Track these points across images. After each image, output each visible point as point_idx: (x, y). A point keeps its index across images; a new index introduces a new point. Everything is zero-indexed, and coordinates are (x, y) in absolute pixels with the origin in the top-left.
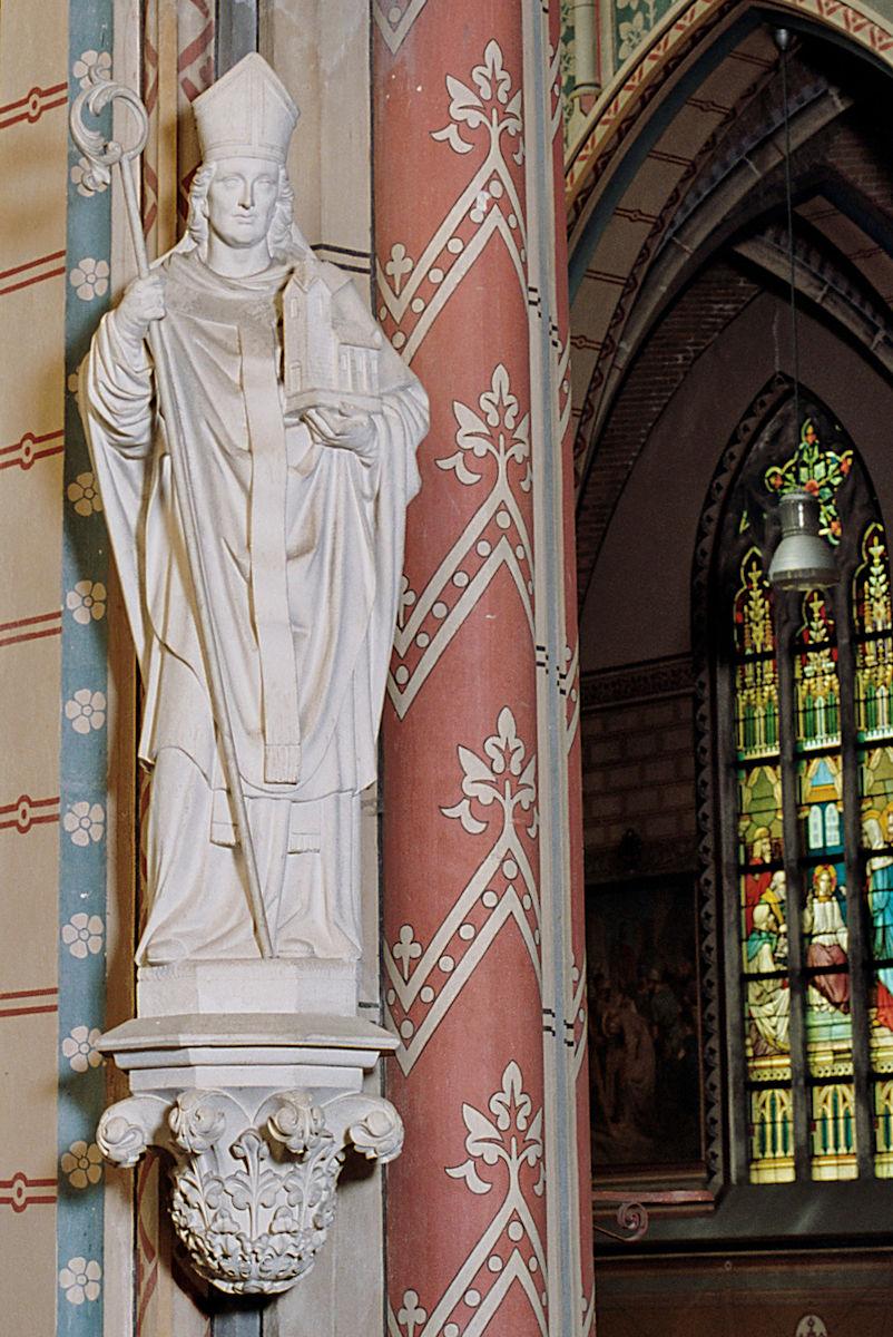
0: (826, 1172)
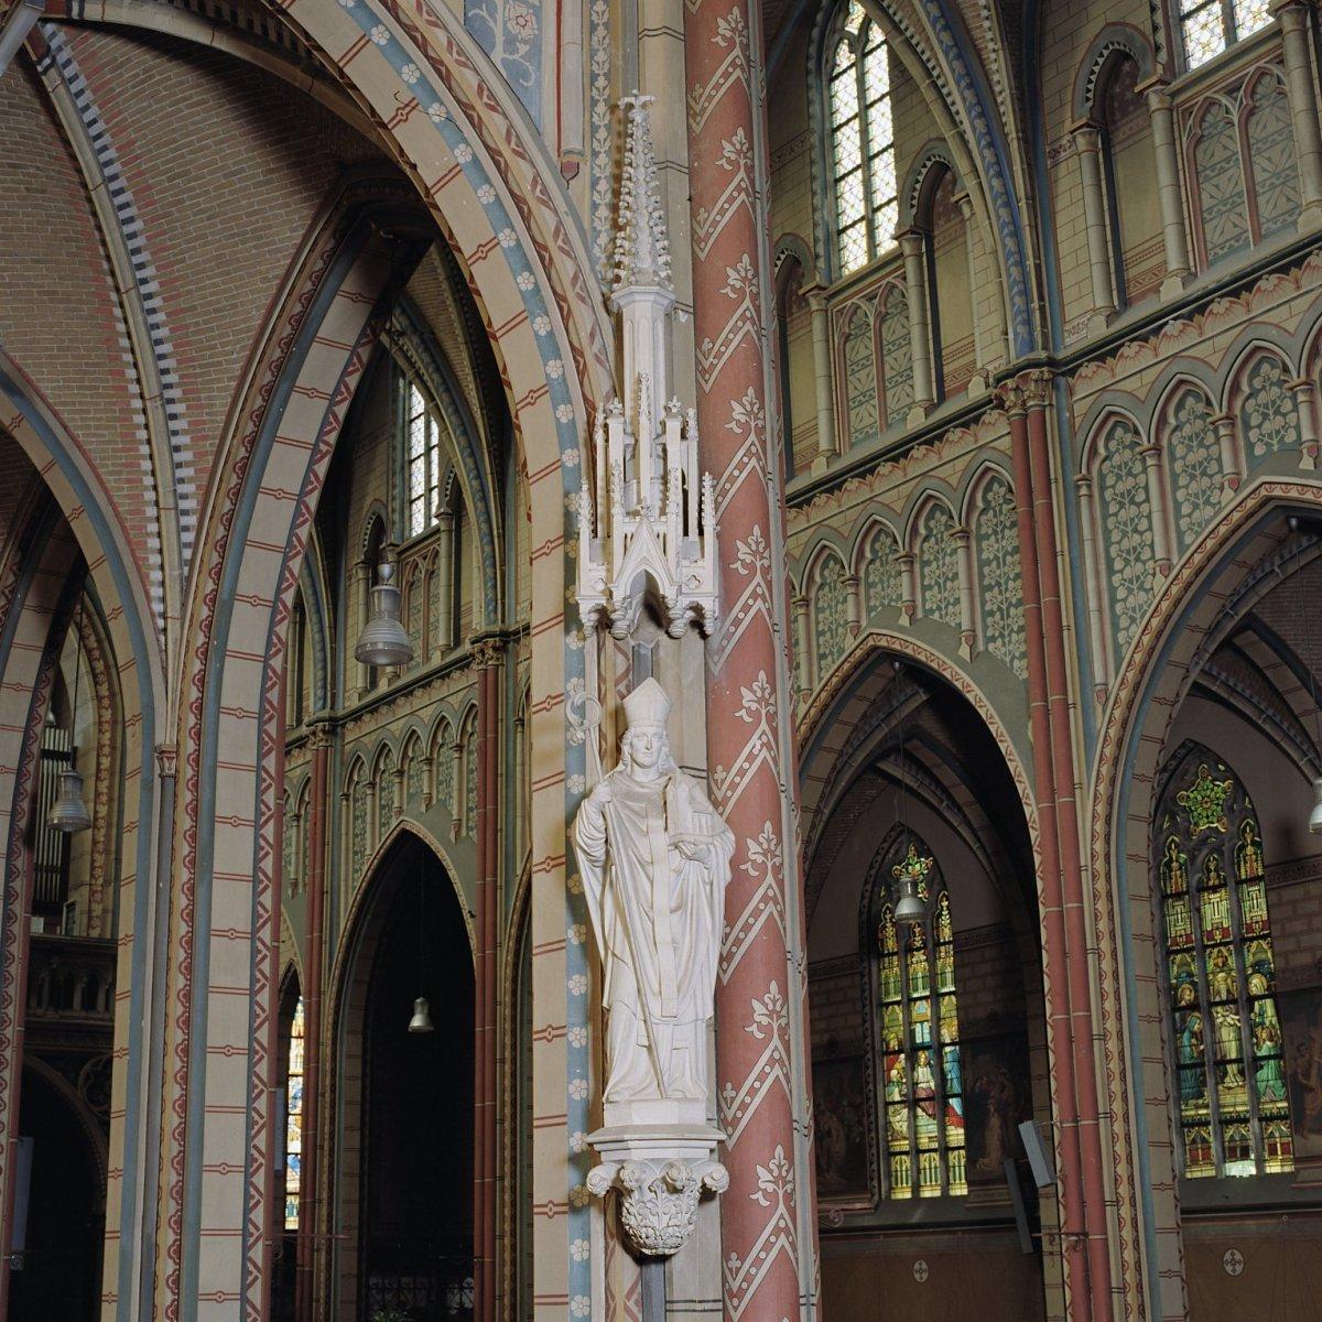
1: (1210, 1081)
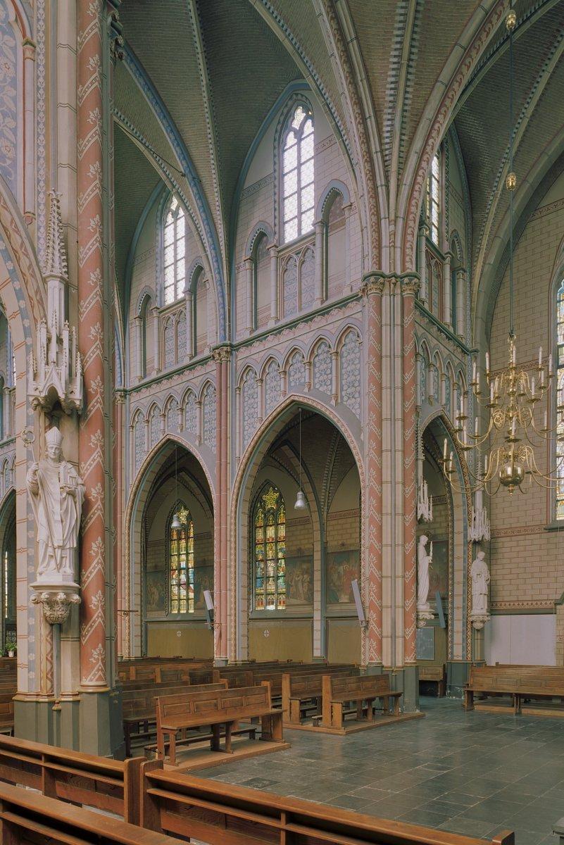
0: (182, 612)
1: (265, 583)
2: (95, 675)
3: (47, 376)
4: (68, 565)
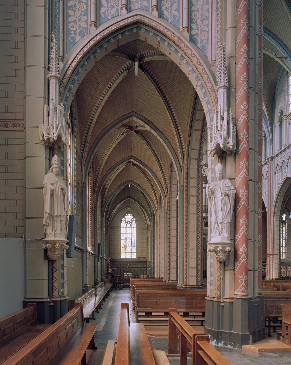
2: (240, 289)
3: (215, 138)
4: (225, 232)
